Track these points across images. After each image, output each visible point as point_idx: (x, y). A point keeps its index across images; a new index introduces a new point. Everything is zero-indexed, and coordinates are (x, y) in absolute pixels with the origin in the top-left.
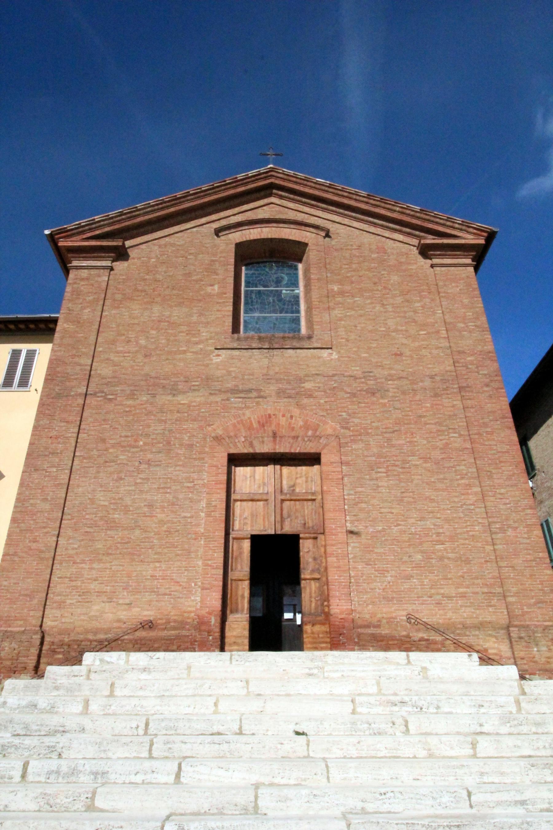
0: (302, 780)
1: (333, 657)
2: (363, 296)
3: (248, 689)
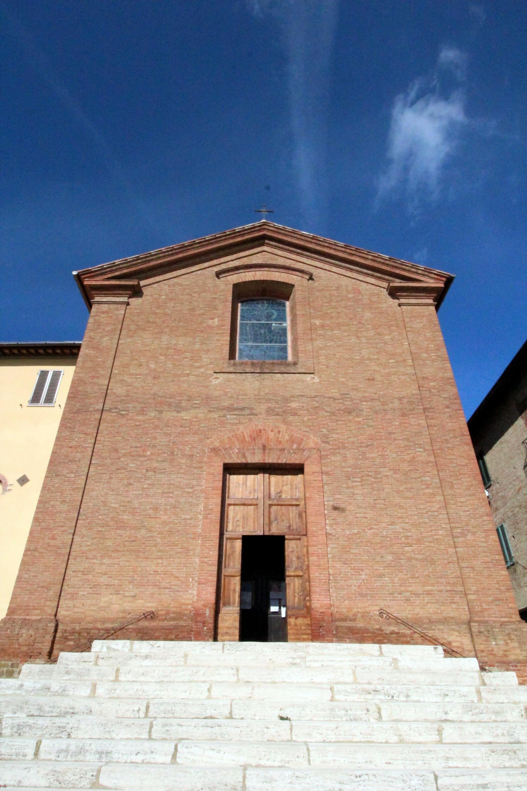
2: (340, 329)
3: (238, 676)
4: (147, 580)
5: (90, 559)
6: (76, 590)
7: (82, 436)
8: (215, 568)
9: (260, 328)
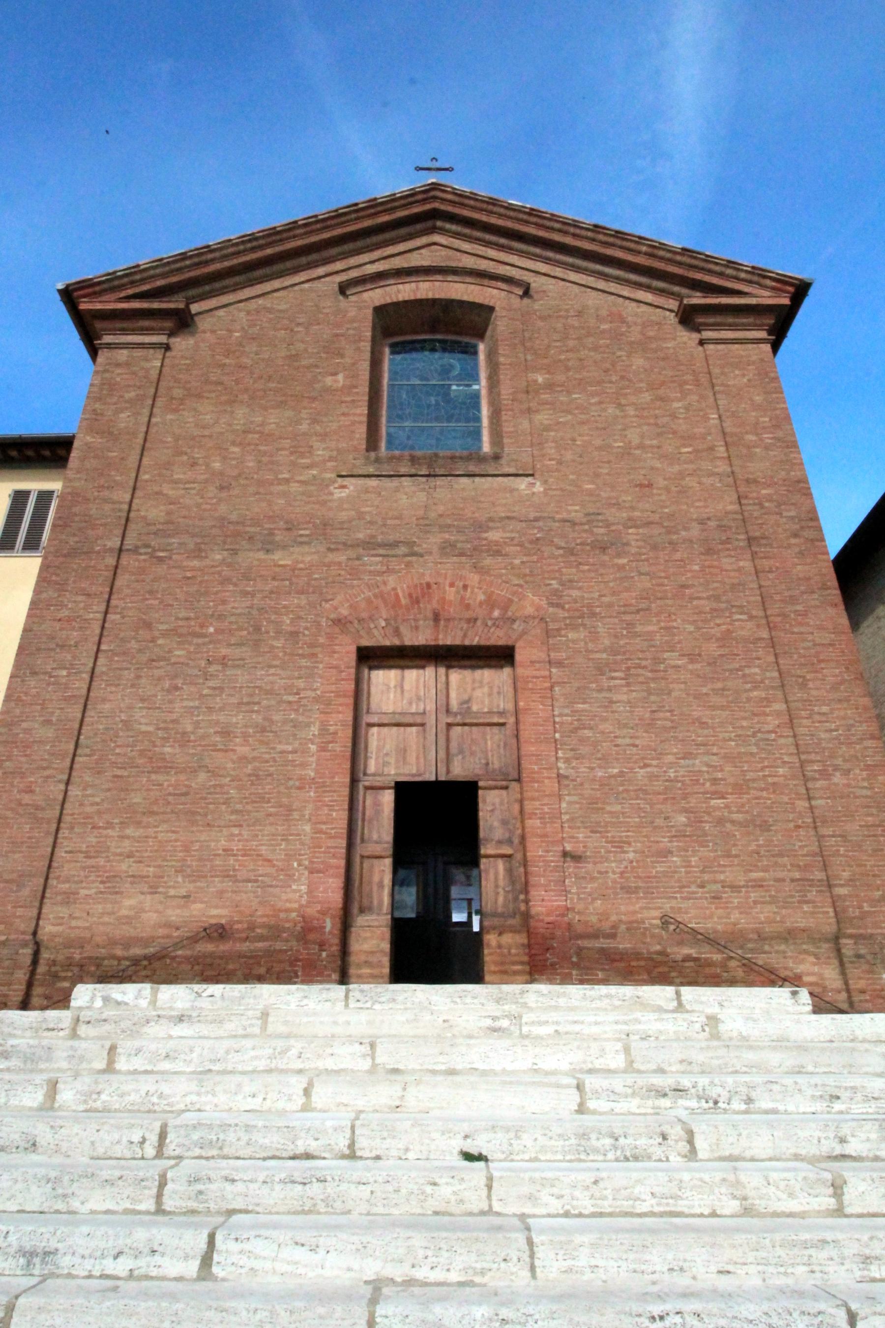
3: (373, 1059)
4: (212, 866)
5: (100, 828)
6: (73, 886)
7: (80, 598)
8: (343, 843)
9: (428, 394)
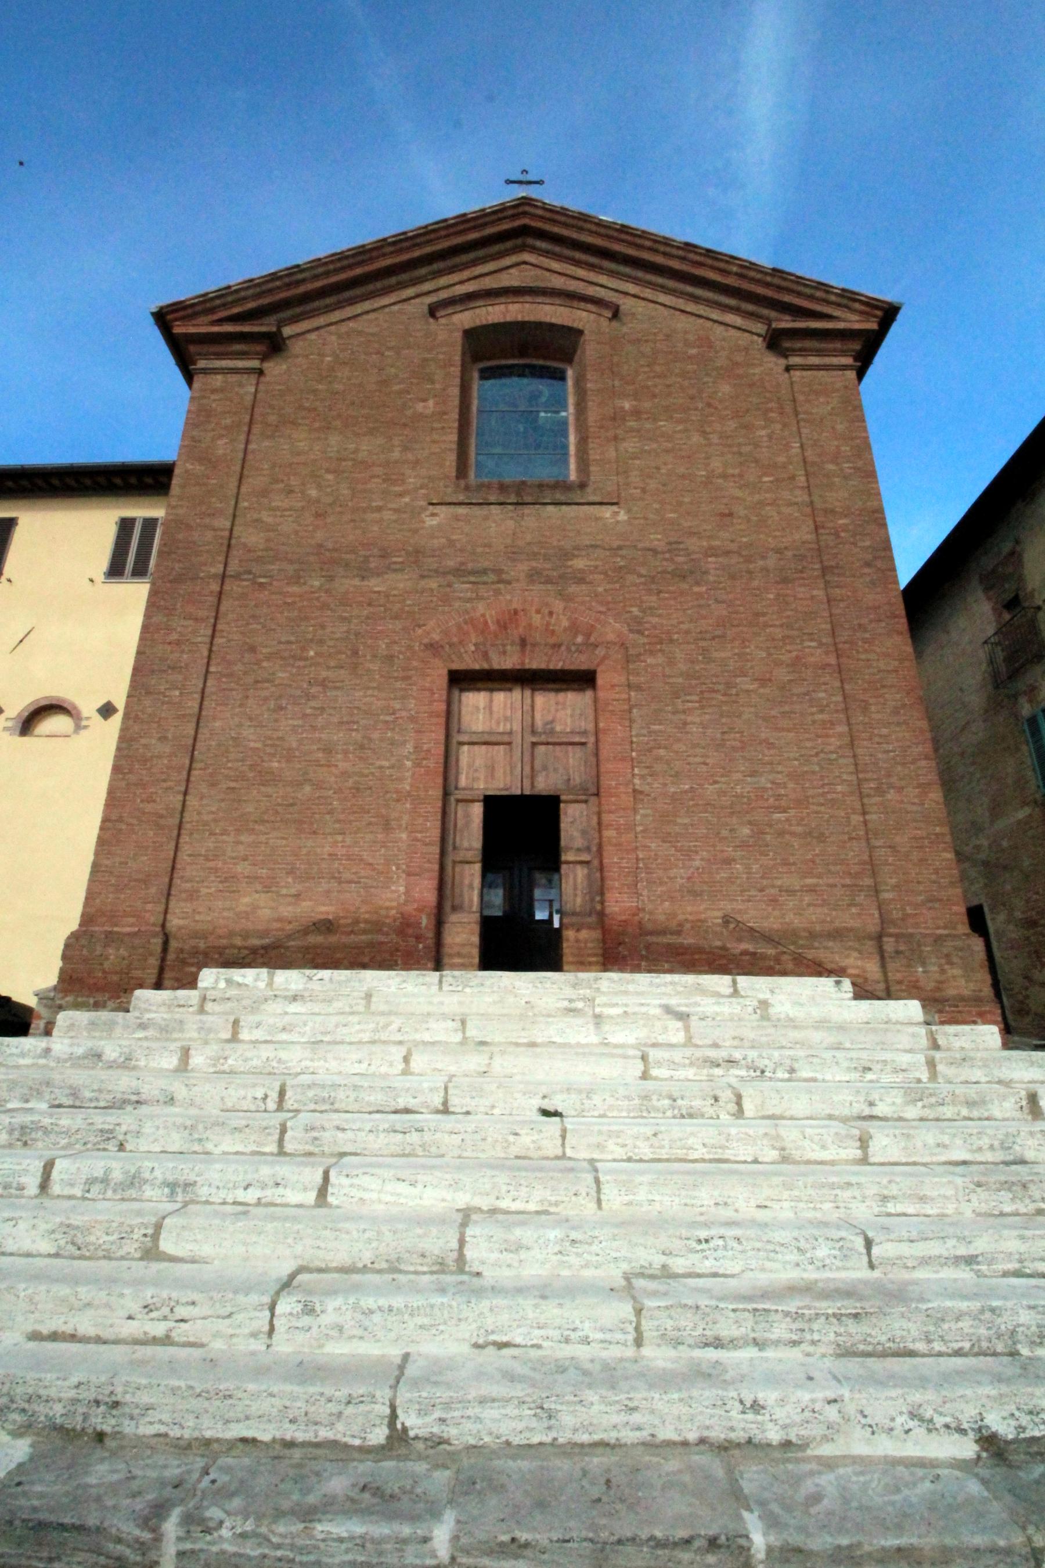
0: (550, 1205)
1: (611, 981)
2: (671, 417)
3: (464, 1032)
7: (190, 622)
